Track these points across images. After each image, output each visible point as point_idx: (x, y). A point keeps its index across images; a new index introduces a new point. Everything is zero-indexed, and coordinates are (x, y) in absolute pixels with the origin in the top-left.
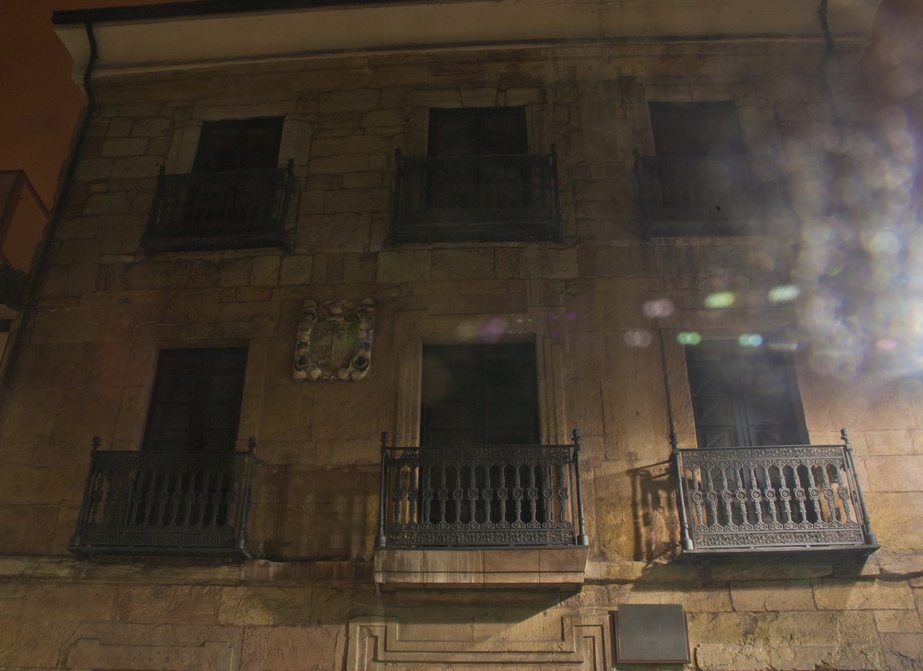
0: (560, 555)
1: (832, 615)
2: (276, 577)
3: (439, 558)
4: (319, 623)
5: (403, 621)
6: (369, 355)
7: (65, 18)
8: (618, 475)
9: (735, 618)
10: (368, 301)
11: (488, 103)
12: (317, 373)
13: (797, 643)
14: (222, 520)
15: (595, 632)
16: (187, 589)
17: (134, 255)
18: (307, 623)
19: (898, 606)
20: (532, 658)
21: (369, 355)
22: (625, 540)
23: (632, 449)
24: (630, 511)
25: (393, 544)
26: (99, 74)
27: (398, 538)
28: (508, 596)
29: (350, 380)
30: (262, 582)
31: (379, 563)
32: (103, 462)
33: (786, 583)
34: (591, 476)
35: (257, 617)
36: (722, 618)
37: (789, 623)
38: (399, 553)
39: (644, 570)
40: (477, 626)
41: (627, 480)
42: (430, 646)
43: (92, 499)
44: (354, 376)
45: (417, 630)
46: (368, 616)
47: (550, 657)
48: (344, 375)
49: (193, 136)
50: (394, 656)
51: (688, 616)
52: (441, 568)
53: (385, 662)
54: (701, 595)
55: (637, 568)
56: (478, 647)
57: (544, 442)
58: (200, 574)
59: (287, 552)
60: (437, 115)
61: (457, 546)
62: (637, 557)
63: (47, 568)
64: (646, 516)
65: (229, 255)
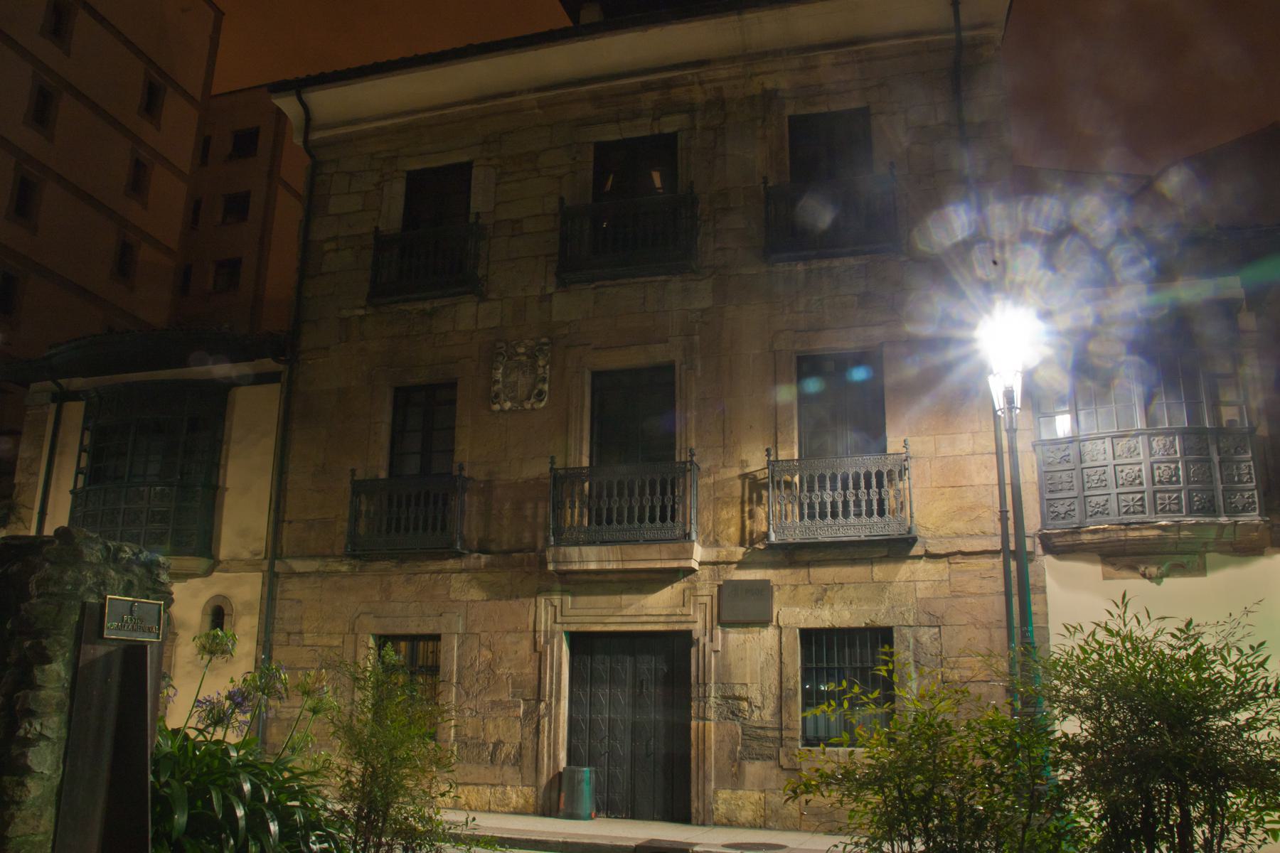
0: (674, 547)
1: (882, 586)
2: (486, 566)
4: (517, 597)
5: (574, 594)
6: (546, 387)
7: (280, 87)
8: (732, 479)
9: (811, 589)
10: (544, 340)
11: (644, 133)
12: (508, 405)
13: (854, 607)
14: (443, 528)
15: (707, 600)
16: (427, 576)
17: (364, 308)
18: (509, 598)
19: (936, 577)
20: (662, 619)
21: (546, 387)
22: (734, 531)
23: (744, 457)
24: (739, 508)
25: (558, 544)
26: (315, 136)
27: (563, 537)
28: (644, 576)
29: (533, 409)
30: (477, 570)
31: (549, 555)
32: (359, 488)
33: (853, 562)
34: (711, 480)
35: (476, 594)
36: (801, 589)
37: (851, 592)
38: (562, 549)
39: (744, 554)
40: (624, 597)
41: (739, 483)
42: (591, 612)
43: (355, 518)
44: (536, 406)
45: (583, 600)
46: (549, 591)
47: (674, 619)
48: (528, 406)
49: (398, 188)
50: (568, 619)
51: (775, 588)
52: (591, 559)
53: (562, 623)
54: (787, 572)
55: (739, 553)
57: (677, 459)
58: (434, 566)
59: (493, 547)
60: (602, 149)
61: (604, 543)
62: (742, 544)
63: (334, 566)
64: (751, 511)
65: (436, 303)
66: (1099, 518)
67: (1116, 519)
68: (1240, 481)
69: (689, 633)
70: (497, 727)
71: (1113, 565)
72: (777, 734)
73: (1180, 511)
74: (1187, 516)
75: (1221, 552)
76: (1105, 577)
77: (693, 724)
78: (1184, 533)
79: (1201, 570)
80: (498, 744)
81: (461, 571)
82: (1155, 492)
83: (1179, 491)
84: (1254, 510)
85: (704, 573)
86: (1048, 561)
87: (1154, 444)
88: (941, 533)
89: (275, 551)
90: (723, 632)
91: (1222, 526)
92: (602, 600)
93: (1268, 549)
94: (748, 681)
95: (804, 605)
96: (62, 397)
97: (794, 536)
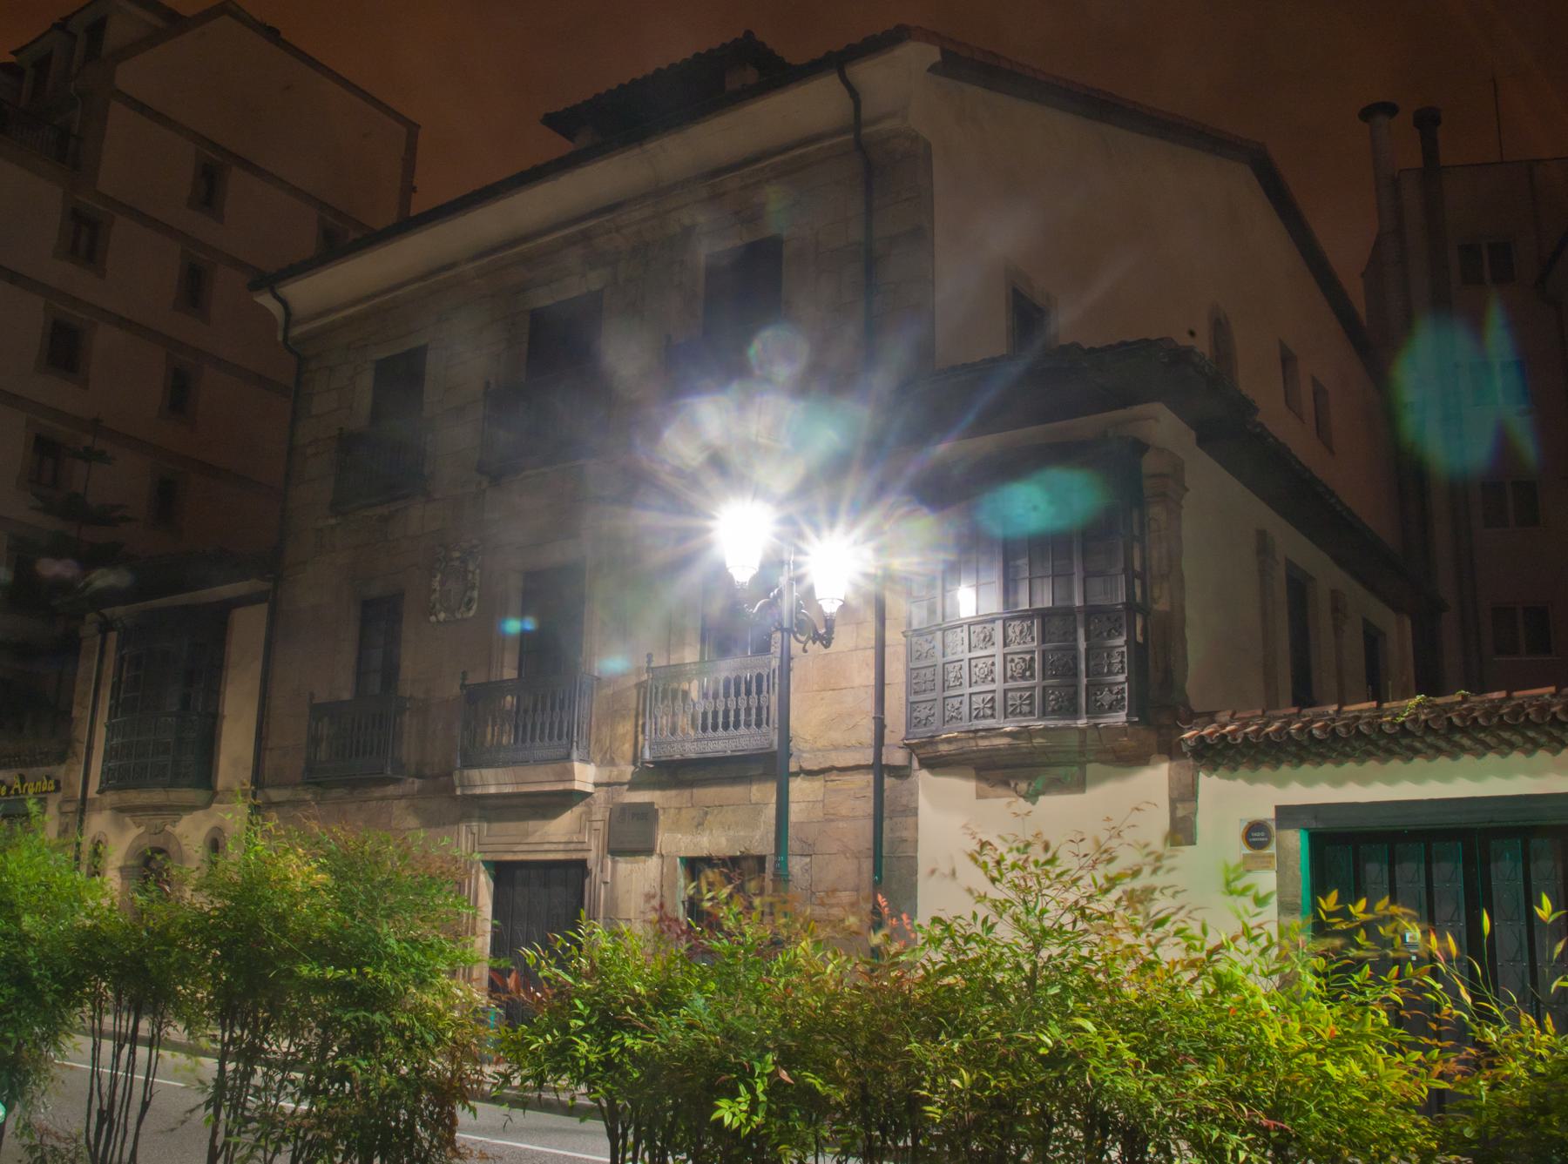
0: (557, 767)
3: (489, 774)
5: (489, 821)
12: (442, 616)
15: (599, 825)
20: (561, 847)
21: (475, 594)
24: (633, 720)
33: (735, 780)
38: (466, 772)
41: (634, 692)
42: (504, 839)
45: (496, 826)
47: (572, 846)
50: (486, 848)
52: (491, 782)
54: (673, 793)
56: (530, 840)
58: (377, 793)
61: (505, 764)
66: (954, 724)
67: (965, 725)
68: (1110, 673)
71: (986, 780)
73: (1031, 713)
74: (1039, 719)
75: (1103, 762)
76: (979, 796)
78: (1038, 741)
79: (1080, 785)
81: (401, 797)
82: (1006, 691)
83: (1032, 688)
84: (1122, 708)
85: (601, 795)
86: (923, 777)
87: (1010, 630)
88: (819, 745)
89: (258, 780)
90: (614, 862)
91: (1082, 731)
92: (512, 827)
93: (1154, 757)
94: (632, 916)
95: (692, 829)
96: (106, 627)
97: (691, 750)
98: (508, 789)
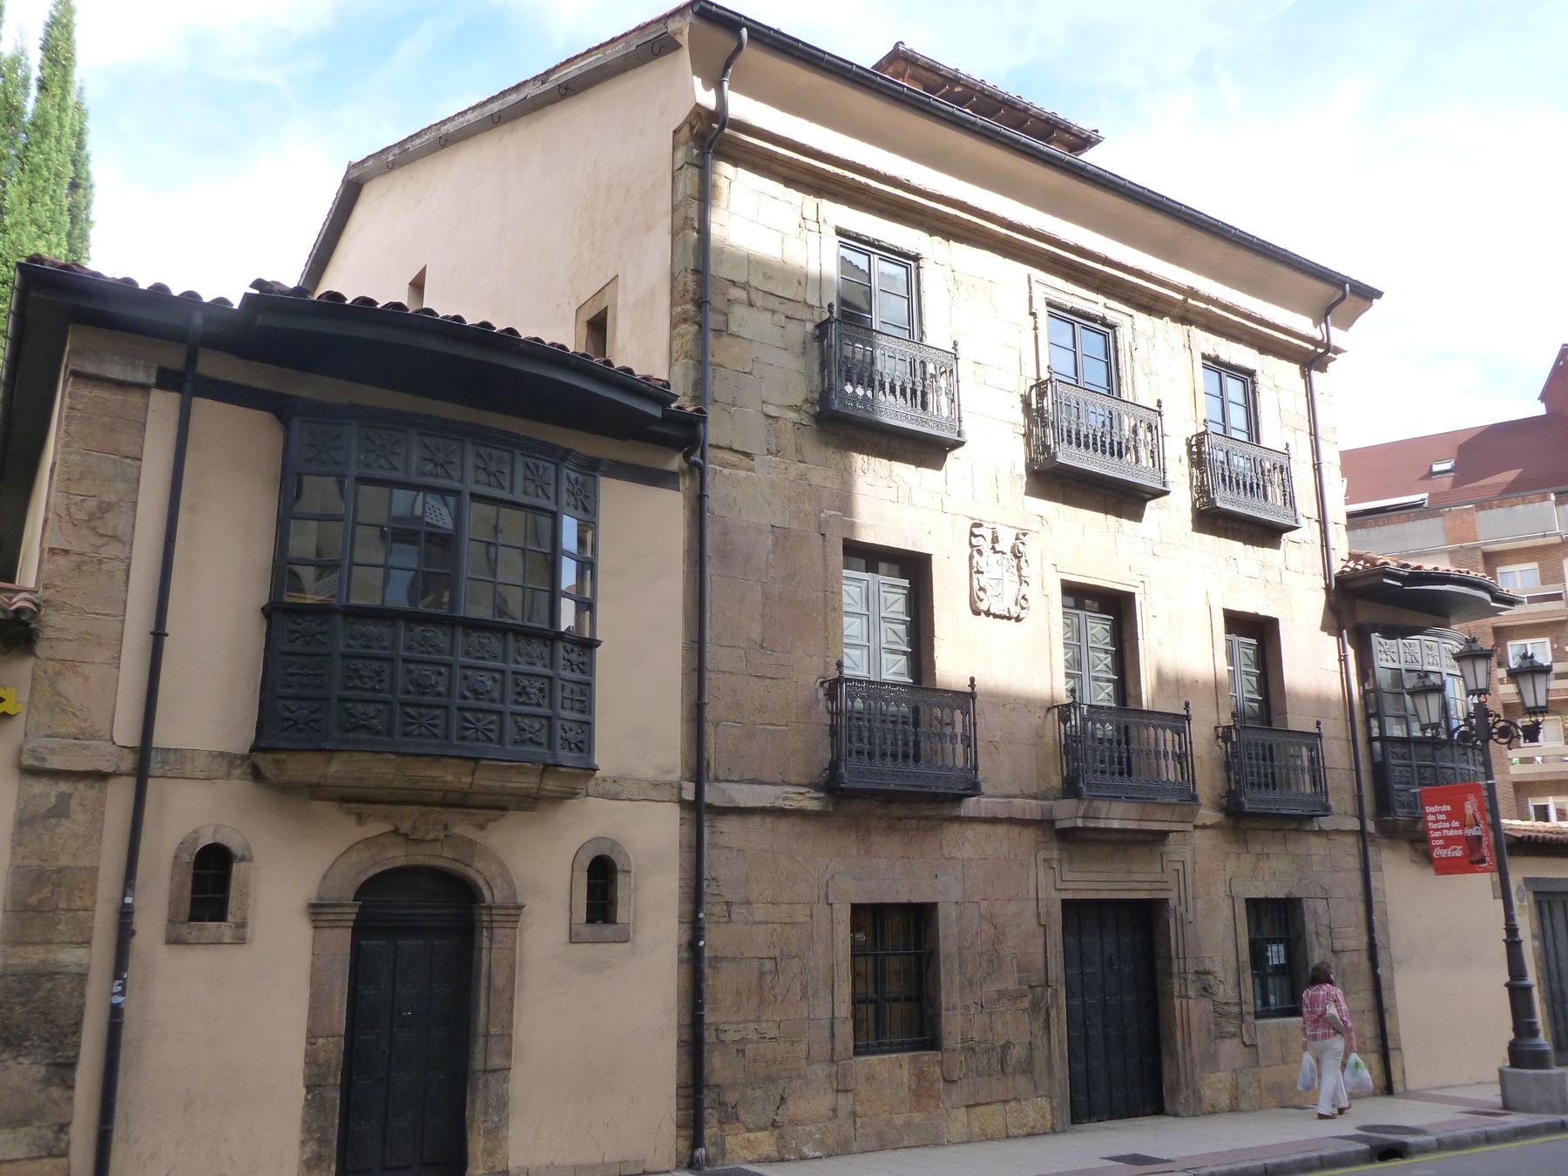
50: (1068, 885)
69: (1166, 901)
70: (1005, 1024)
72: (1235, 1009)
77: (1177, 1002)
80: (1007, 1046)
98: (1131, 825)
